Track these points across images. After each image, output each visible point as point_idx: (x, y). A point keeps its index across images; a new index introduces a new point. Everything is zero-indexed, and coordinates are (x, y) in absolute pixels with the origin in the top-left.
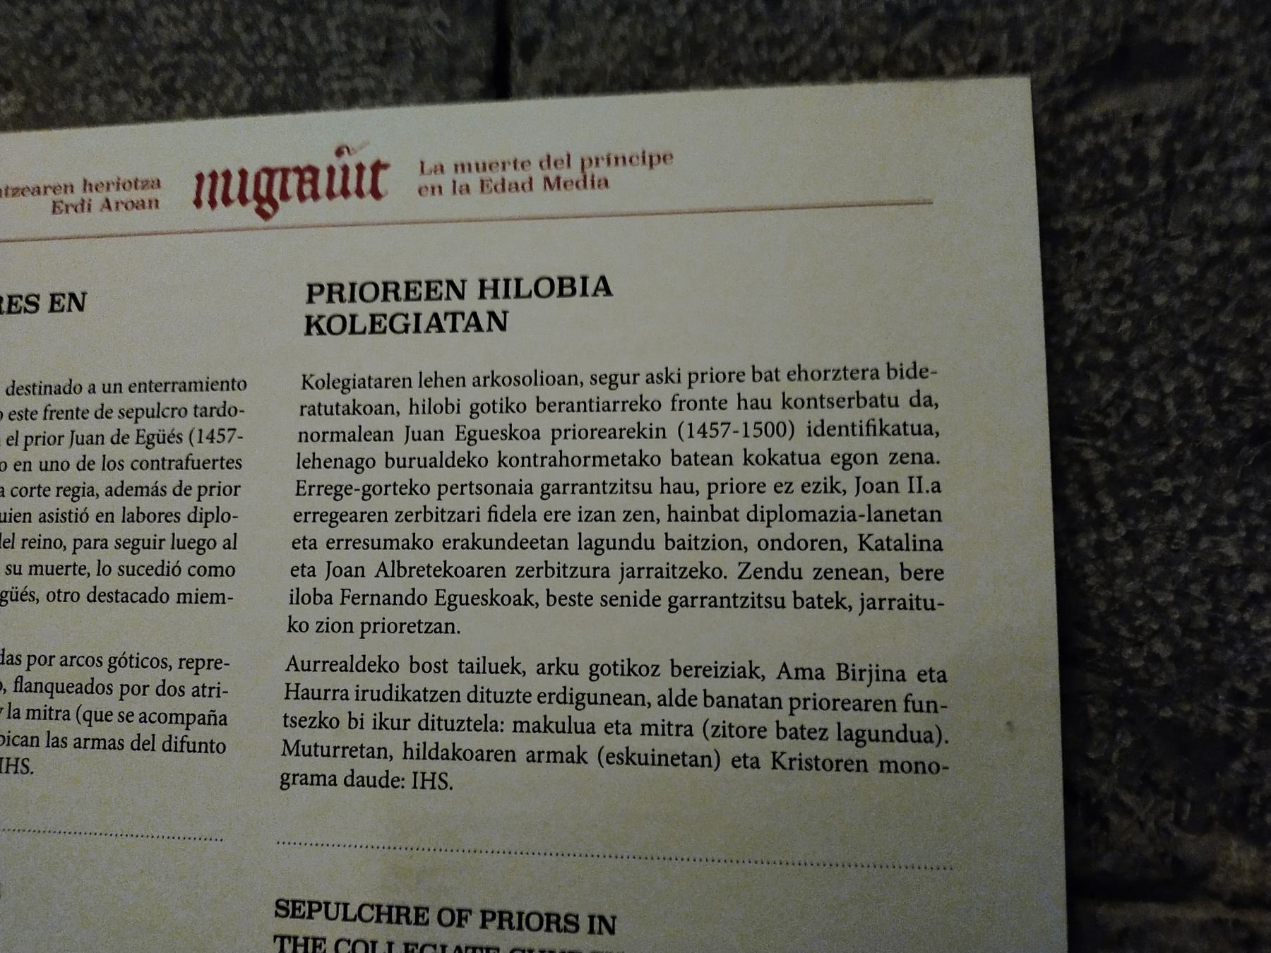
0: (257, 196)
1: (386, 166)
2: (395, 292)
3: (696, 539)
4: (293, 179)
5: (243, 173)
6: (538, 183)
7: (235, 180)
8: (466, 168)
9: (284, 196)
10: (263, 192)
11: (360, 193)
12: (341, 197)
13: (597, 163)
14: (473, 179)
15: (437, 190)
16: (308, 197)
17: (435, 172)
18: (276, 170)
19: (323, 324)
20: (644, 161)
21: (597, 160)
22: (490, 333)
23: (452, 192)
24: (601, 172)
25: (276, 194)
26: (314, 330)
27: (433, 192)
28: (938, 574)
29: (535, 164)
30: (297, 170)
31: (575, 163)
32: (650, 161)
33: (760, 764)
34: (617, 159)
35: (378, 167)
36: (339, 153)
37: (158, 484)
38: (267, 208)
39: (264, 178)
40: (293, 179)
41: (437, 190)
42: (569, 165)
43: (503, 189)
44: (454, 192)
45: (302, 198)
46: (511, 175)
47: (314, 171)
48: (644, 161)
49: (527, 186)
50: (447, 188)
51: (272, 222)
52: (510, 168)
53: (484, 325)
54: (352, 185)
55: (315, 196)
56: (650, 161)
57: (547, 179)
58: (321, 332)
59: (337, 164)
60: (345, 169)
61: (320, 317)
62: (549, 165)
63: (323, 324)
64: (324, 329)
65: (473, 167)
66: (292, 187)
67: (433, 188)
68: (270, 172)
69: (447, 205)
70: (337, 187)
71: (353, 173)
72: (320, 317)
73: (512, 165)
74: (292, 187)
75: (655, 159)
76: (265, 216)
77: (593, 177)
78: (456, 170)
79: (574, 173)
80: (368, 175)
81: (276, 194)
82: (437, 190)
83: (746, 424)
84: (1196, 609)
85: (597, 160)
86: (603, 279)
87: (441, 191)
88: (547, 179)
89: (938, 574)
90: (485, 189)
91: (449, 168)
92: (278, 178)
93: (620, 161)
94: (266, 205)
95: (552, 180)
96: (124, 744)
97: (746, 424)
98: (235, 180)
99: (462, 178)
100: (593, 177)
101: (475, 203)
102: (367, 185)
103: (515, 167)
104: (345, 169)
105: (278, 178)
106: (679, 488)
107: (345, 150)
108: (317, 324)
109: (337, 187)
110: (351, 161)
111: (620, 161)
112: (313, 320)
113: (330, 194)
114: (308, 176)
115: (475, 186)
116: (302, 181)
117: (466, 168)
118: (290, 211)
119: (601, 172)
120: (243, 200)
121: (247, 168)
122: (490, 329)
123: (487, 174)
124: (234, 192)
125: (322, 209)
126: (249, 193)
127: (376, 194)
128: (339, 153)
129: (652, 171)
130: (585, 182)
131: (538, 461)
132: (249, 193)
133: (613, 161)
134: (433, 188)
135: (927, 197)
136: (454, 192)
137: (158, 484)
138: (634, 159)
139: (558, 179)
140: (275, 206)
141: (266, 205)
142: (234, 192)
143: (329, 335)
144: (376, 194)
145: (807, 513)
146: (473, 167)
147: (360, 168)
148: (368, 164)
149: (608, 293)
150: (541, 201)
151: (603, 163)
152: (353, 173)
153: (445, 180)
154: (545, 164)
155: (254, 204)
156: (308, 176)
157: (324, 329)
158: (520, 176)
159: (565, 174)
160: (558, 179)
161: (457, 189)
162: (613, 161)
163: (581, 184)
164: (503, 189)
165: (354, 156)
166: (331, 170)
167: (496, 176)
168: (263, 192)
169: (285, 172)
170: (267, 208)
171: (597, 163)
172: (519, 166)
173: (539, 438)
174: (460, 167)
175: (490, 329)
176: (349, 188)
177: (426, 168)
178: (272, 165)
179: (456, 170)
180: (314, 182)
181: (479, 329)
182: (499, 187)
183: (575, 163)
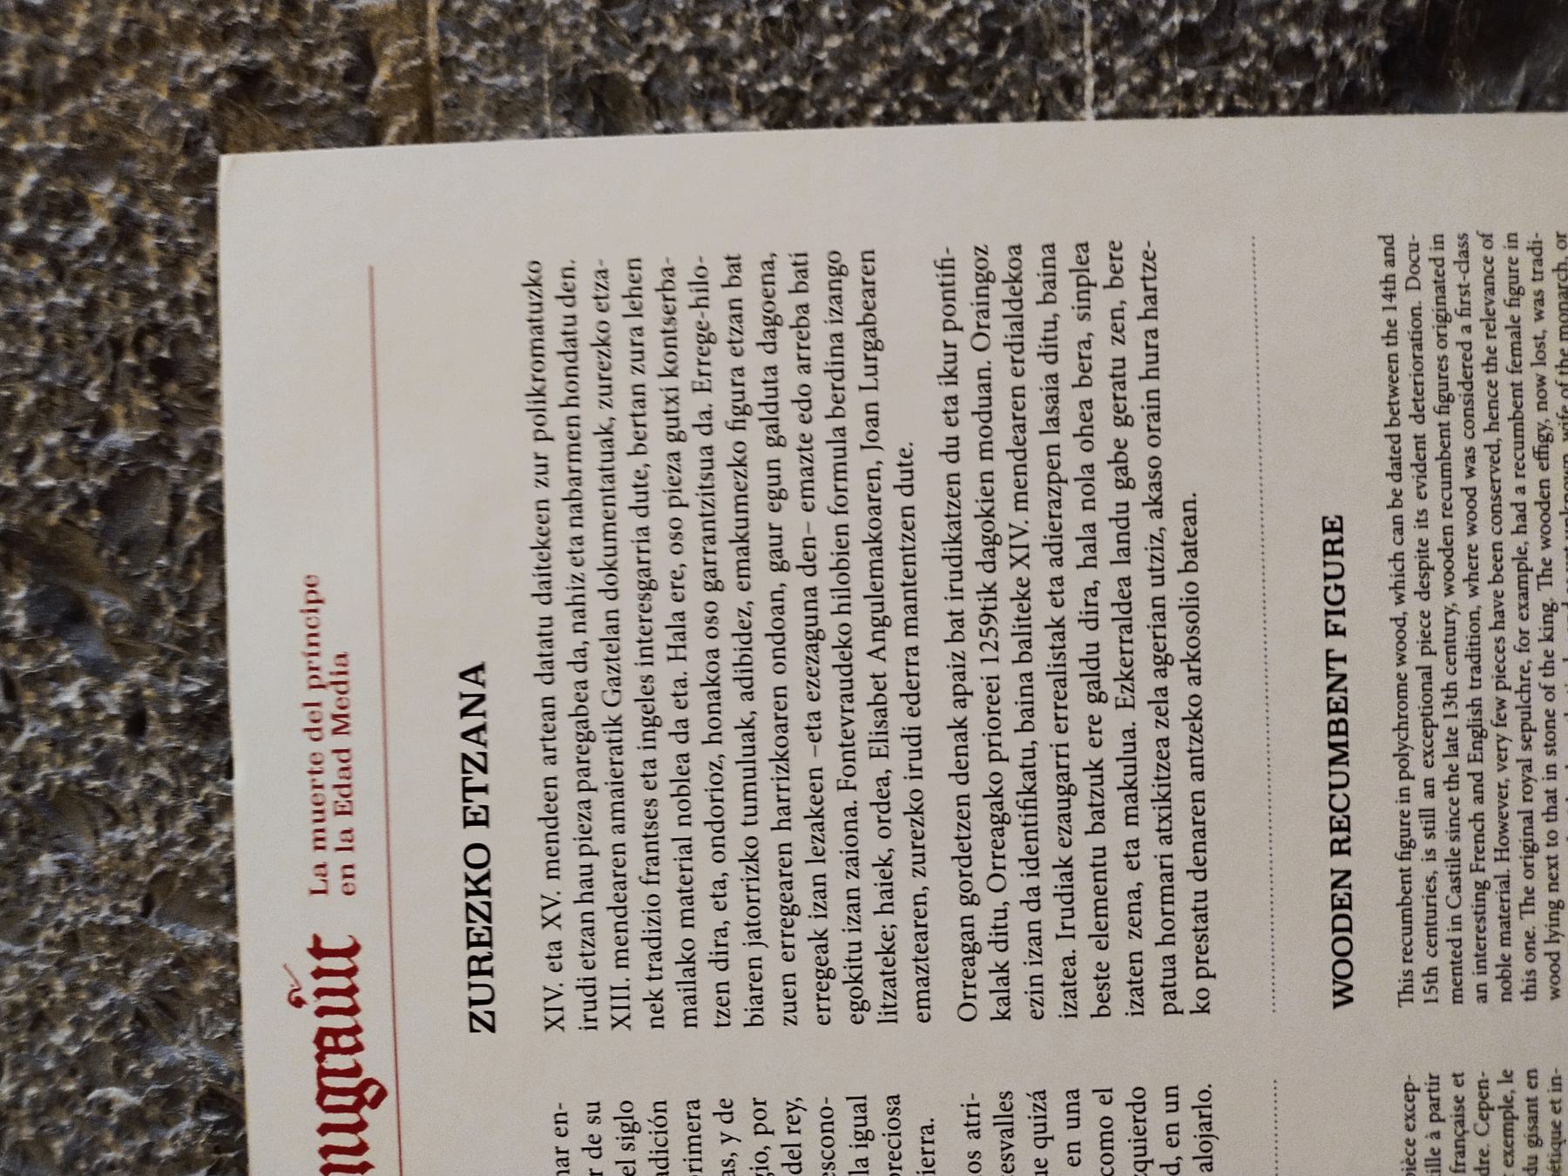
0: (355, 1109)
1: (317, 939)
2: (480, 960)
3: (1158, 778)
4: (332, 1061)
5: (324, 1129)
6: (340, 742)
7: (334, 1139)
8: (320, 835)
9: (356, 1071)
10: (349, 1100)
11: (351, 972)
12: (356, 996)
13: (317, 669)
14: (334, 825)
15: (348, 871)
16: (354, 1000)
17: (324, 875)
18: (320, 1084)
19: (476, 874)
20: (315, 611)
21: (311, 669)
22: (488, 715)
23: (377, 274)
24: (327, 663)
25: (352, 1083)
26: (484, 886)
27: (351, 876)
28: (1115, 247)
29: (316, 747)
30: (320, 1058)
31: (316, 695)
32: (314, 602)
33: (1126, 576)
34: (312, 644)
35: (318, 951)
36: (299, 1003)
37: (652, 1119)
38: (370, 1093)
39: (330, 1100)
40: (332, 1061)
41: (348, 872)
42: (317, 704)
43: (348, 786)
44: (350, 849)
45: (358, 1047)
46: (330, 776)
47: (323, 1032)
48: (315, 611)
49: (344, 756)
50: (346, 858)
51: (390, 1087)
52: (320, 779)
53: (478, 721)
54: (342, 983)
55: (355, 1030)
56: (314, 602)
57: (335, 731)
58: (487, 876)
59: (313, 1004)
60: (320, 993)
61: (467, 878)
62: (318, 729)
63: (476, 874)
64: (483, 872)
65: (319, 826)
66: (344, 1062)
67: (346, 876)
68: (324, 1091)
69: (367, 859)
70: (344, 1002)
71: (327, 982)
72: (467, 878)
73: (316, 776)
74: (344, 1062)
75: (312, 597)
76: (382, 1094)
77: (331, 673)
78: (323, 848)
79: (328, 697)
80: (328, 963)
81: (352, 1083)
82: (348, 871)
83: (983, 660)
84: (149, 584)
85: (311, 669)
86: (463, 675)
87: (351, 867)
88: (335, 731)
89: (1115, 247)
90: (347, 809)
91: (320, 856)
92: (329, 1082)
93: (314, 640)
94: (368, 1094)
95: (337, 724)
96: (649, 798)
97: (983, 660)
98: (334, 1139)
99: (333, 840)
100: (331, 673)
101: (365, 821)
102: (341, 963)
103: (319, 772)
104: (320, 993)
105: (329, 1082)
106: (1064, 815)
107: (296, 994)
108: (476, 883)
109: (344, 1002)
110: (309, 986)
111: (314, 640)
112: (472, 888)
113: (353, 1010)
114: (329, 1042)
115: (344, 822)
116: (337, 1050)
117: (320, 835)
118: (374, 1063)
119: (327, 663)
120: (361, 1125)
121: (318, 1125)
122: (483, 714)
123: (329, 807)
124: (349, 1140)
125: (373, 1019)
126: (351, 1118)
127: (354, 950)
128: (299, 1003)
129: (327, 601)
130: (340, 683)
131: (973, 1120)
132: (351, 1118)
133: (314, 649)
134: (346, 876)
135: (366, 271)
136: (350, 849)
137: (652, 1119)
138: (312, 623)
139: (335, 717)
140: (370, 1082)
141: (368, 1094)
142: (349, 1140)
143: (489, 866)
144: (354, 950)
145: (1018, 501)
146: (319, 826)
147: (318, 973)
148: (314, 963)
149: (481, 668)
150: (361, 738)
151: (316, 661)
152: (327, 982)
153: (335, 861)
154: (316, 735)
155: (366, 1111)
156: (329, 1042)
157: (483, 872)
158: (332, 764)
159: (330, 707)
160: (335, 717)
161: (347, 845)
162: (314, 649)
163: (342, 688)
164: (348, 786)
165: (304, 984)
166: (321, 1012)
167: (331, 795)
168: (349, 1100)
169: (322, 1073)
170: (370, 1093)
171: (317, 669)
172: (317, 768)
173: (898, 1097)
174: (319, 843)
175: (483, 714)
176: (347, 1006)
177: (321, 887)
178: (314, 1090)
179: (323, 848)
180: (336, 1033)
181: (483, 728)
182: (345, 791)
183: (316, 695)
